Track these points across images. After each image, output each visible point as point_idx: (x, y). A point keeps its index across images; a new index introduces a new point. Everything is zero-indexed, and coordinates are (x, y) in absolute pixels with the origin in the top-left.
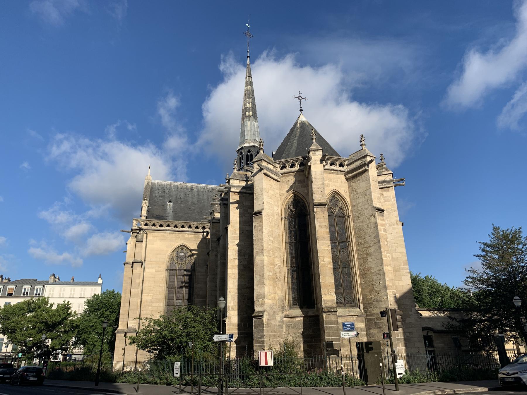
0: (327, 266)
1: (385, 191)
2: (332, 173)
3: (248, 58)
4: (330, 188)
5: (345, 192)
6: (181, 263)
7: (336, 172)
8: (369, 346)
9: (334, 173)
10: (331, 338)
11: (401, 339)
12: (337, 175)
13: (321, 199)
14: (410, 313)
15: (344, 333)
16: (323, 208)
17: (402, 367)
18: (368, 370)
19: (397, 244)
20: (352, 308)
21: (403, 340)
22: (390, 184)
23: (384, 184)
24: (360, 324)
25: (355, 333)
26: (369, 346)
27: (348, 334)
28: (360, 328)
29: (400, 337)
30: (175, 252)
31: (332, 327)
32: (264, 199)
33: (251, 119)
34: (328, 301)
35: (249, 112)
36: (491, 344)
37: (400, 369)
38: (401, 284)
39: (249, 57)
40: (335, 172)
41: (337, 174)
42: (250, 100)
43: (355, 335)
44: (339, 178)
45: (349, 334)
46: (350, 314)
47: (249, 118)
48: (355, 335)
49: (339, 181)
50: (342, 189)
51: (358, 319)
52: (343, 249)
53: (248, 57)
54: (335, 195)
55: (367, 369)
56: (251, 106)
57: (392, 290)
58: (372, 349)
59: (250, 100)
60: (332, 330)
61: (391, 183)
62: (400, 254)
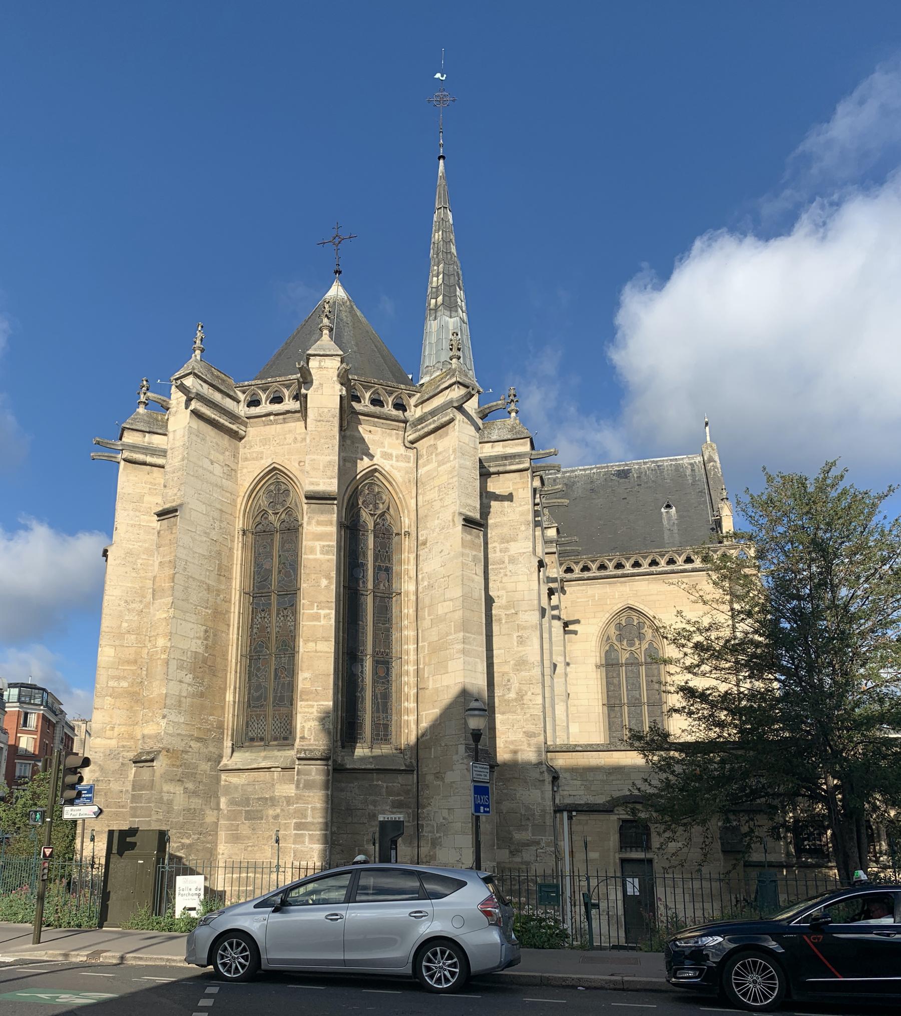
0: (159, 656)
1: (441, 437)
2: (272, 423)
3: (441, 161)
4: (263, 462)
5: (302, 464)
6: (629, 649)
7: (281, 417)
8: (128, 839)
9: (276, 422)
10: (137, 819)
11: (313, 824)
12: (286, 425)
13: (176, 497)
14: (455, 757)
15: (72, 810)
16: (172, 519)
17: (198, 892)
18: (111, 894)
19: (448, 576)
20: (279, 750)
21: (319, 826)
22: (446, 415)
23: (435, 418)
24: (286, 786)
25: (95, 809)
26: (128, 839)
27: (79, 812)
28: (285, 797)
29: (309, 819)
30: (613, 626)
31: (141, 796)
32: (529, 494)
33: (439, 314)
34: (149, 738)
35: (436, 299)
36: (877, 848)
37: (190, 897)
38: (445, 684)
39: (443, 157)
40: (277, 417)
41: (285, 421)
42: (441, 266)
43: (94, 813)
44: (290, 431)
45: (82, 812)
46: (263, 765)
47: (436, 312)
48: (94, 813)
49: (290, 438)
50: (293, 457)
51: (283, 775)
52: (285, 609)
53: (439, 158)
54: (279, 477)
55: (109, 892)
56: (440, 281)
57: (316, 701)
58: (133, 846)
59: (441, 266)
60: (141, 803)
61: (450, 410)
62: (451, 603)
